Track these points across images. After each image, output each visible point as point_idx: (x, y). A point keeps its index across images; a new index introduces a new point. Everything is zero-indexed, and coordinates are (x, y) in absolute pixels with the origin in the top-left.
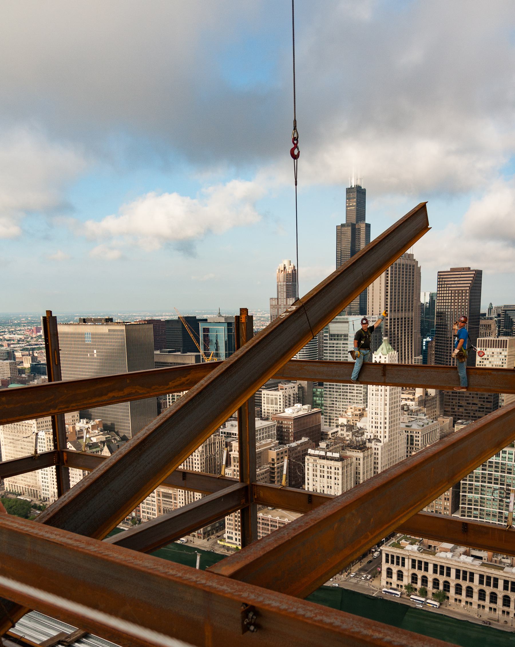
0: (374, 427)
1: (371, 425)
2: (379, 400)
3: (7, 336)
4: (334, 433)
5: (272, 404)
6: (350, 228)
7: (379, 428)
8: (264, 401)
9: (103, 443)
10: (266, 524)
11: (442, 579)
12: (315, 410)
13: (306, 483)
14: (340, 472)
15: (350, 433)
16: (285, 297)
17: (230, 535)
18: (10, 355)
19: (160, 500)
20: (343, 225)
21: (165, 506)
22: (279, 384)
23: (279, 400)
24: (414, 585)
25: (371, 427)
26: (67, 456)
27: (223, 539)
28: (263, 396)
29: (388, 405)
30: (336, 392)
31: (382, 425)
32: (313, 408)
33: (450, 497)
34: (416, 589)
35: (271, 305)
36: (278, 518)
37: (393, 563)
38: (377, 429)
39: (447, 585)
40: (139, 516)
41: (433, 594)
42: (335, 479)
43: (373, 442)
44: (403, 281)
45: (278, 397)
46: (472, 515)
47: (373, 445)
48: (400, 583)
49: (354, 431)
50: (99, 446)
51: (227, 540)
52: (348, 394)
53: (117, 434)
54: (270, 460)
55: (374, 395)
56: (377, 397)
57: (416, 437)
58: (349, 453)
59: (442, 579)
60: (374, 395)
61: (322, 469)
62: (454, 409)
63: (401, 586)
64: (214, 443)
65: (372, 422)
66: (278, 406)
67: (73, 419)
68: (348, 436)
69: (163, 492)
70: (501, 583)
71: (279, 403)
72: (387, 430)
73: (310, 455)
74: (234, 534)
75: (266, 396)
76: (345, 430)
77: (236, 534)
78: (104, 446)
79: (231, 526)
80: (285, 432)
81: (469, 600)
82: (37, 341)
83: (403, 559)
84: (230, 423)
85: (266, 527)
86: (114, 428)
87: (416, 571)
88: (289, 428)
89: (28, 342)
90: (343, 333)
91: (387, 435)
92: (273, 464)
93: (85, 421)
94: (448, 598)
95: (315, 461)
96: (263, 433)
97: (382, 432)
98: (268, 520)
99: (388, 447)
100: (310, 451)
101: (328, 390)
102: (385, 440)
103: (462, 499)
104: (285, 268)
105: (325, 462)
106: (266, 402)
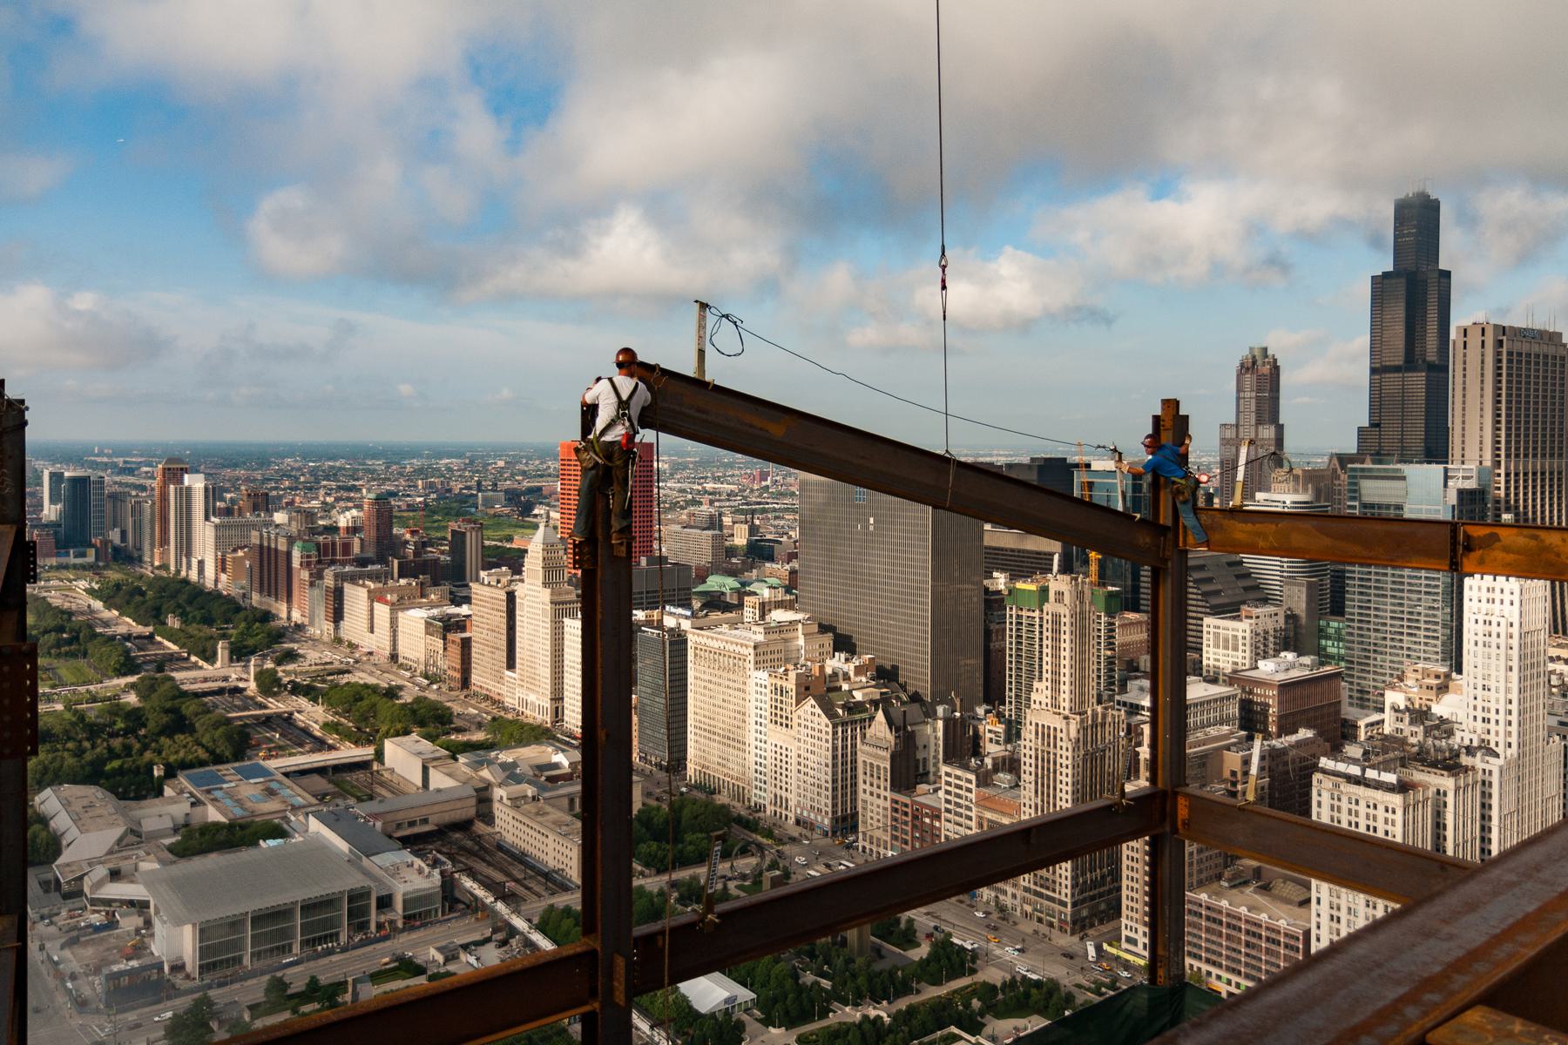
3: (709, 486)
4: (1372, 724)
5: (1226, 648)
6: (1403, 280)
9: (875, 703)
10: (1214, 920)
12: (1328, 669)
14: (1399, 817)
15: (1420, 729)
16: (1253, 422)
17: (1132, 935)
18: (714, 523)
20: (1386, 275)
26: (1191, 808)
27: (1115, 939)
28: (1205, 629)
29: (1516, 669)
30: (1376, 630)
31: (1501, 717)
32: (1322, 664)
35: (1222, 439)
36: (1243, 910)
38: (1486, 726)
43: (1479, 755)
44: (1536, 390)
45: (1240, 634)
47: (1477, 761)
49: (1428, 723)
50: (866, 710)
51: (1125, 945)
52: (1405, 638)
53: (903, 687)
54: (1227, 774)
58: (1418, 776)
60: (1480, 644)
64: (1103, 725)
65: (1475, 708)
66: (1240, 654)
68: (1415, 735)
69: (989, 821)
71: (1241, 647)
72: (1514, 728)
73: (1324, 771)
75: (1212, 630)
76: (1407, 720)
78: (877, 709)
79: (1134, 915)
82: (760, 496)
84: (1138, 682)
85: (1214, 926)
86: (897, 675)
89: (744, 498)
90: (1393, 501)
91: (1514, 740)
92: (1234, 784)
96: (1209, 712)
98: (1220, 912)
99: (1519, 768)
100: (1325, 762)
101: (1356, 625)
102: (1509, 751)
104: (1254, 363)
105: (1360, 791)
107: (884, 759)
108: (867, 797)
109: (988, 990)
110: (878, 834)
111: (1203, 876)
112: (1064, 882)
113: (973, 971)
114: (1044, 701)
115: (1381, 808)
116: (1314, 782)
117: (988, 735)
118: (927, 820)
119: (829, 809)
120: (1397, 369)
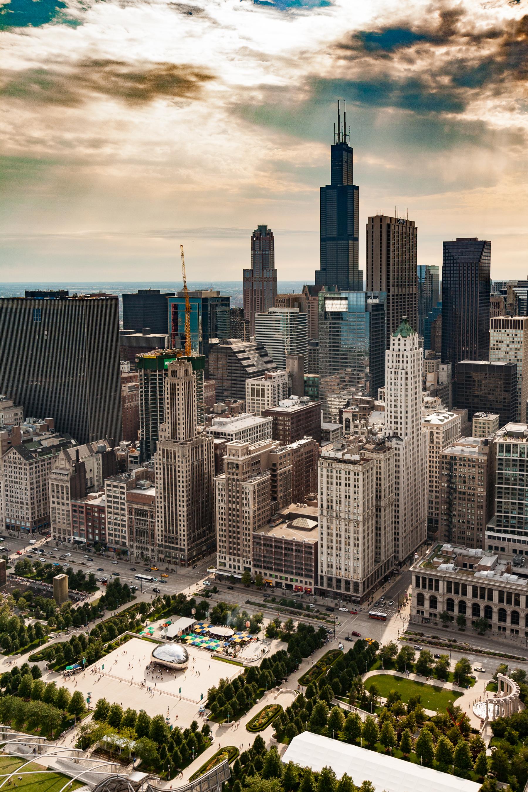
0: (393, 423)
1: (389, 420)
2: (399, 390)
7: (399, 423)
8: (248, 392)
11: (483, 604)
13: (319, 493)
14: (361, 477)
19: (132, 518)
21: (139, 526)
22: (266, 372)
23: (266, 392)
24: (450, 613)
25: (389, 422)
28: (247, 386)
31: (403, 421)
33: (484, 504)
34: (452, 618)
37: (424, 587)
39: (489, 611)
40: (105, 540)
41: (473, 622)
42: (355, 486)
45: (266, 388)
46: (510, 525)
47: (393, 443)
48: (433, 611)
55: (393, 384)
56: (396, 387)
57: (437, 433)
59: (483, 604)
60: (393, 384)
61: (347, 476)
62: (468, 400)
63: (435, 615)
66: (266, 399)
67: (16, 417)
69: (136, 509)
70: (469, 589)
74: (227, 559)
75: (250, 386)
77: (230, 559)
79: (224, 550)
80: (280, 430)
81: (515, 627)
83: (437, 582)
87: (452, 595)
88: (285, 425)
93: (32, 420)
94: (490, 626)
95: (330, 465)
97: (403, 429)
103: (498, 506)
105: (342, 466)
106: (250, 394)
107: (66, 481)
108: (56, 505)
109: (142, 608)
110: (64, 527)
111: (260, 523)
112: (182, 538)
113: (135, 598)
114: (167, 435)
115: (352, 474)
116: (319, 465)
117: (129, 459)
118: (96, 514)
119: (30, 516)
120: (333, 239)
